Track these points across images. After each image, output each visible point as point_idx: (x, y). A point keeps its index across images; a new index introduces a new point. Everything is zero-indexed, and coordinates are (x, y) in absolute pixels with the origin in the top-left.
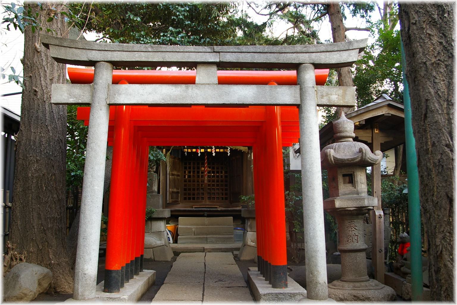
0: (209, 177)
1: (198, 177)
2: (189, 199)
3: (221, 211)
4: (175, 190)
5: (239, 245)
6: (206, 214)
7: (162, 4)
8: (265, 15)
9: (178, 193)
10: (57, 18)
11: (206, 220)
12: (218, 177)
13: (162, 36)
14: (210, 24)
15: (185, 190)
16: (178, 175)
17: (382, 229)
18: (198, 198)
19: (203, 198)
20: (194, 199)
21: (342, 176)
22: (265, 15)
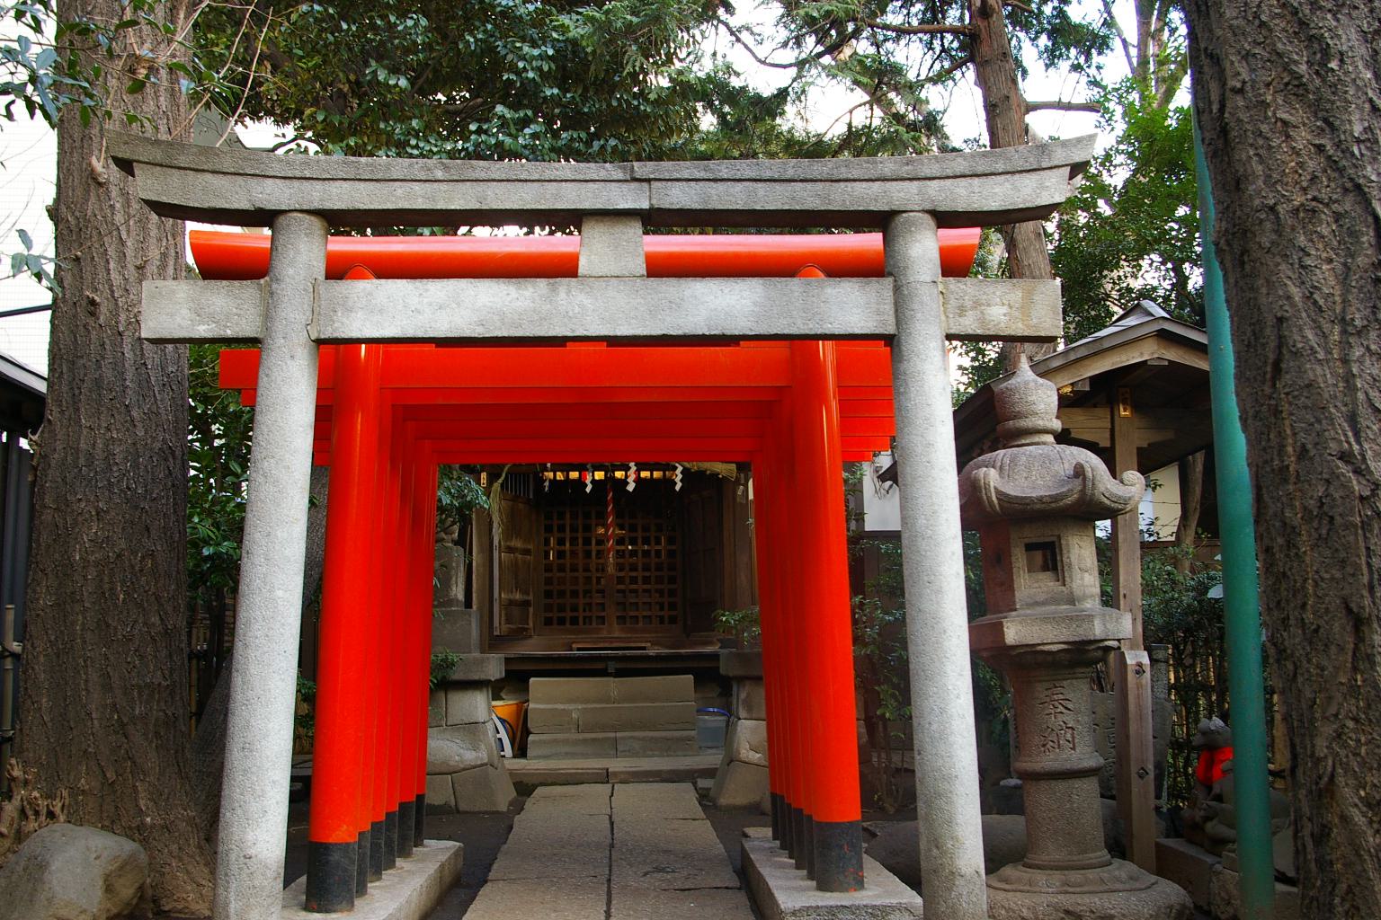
0: (620, 554)
2: (561, 621)
6: (612, 667)
12: (646, 554)
15: (548, 594)
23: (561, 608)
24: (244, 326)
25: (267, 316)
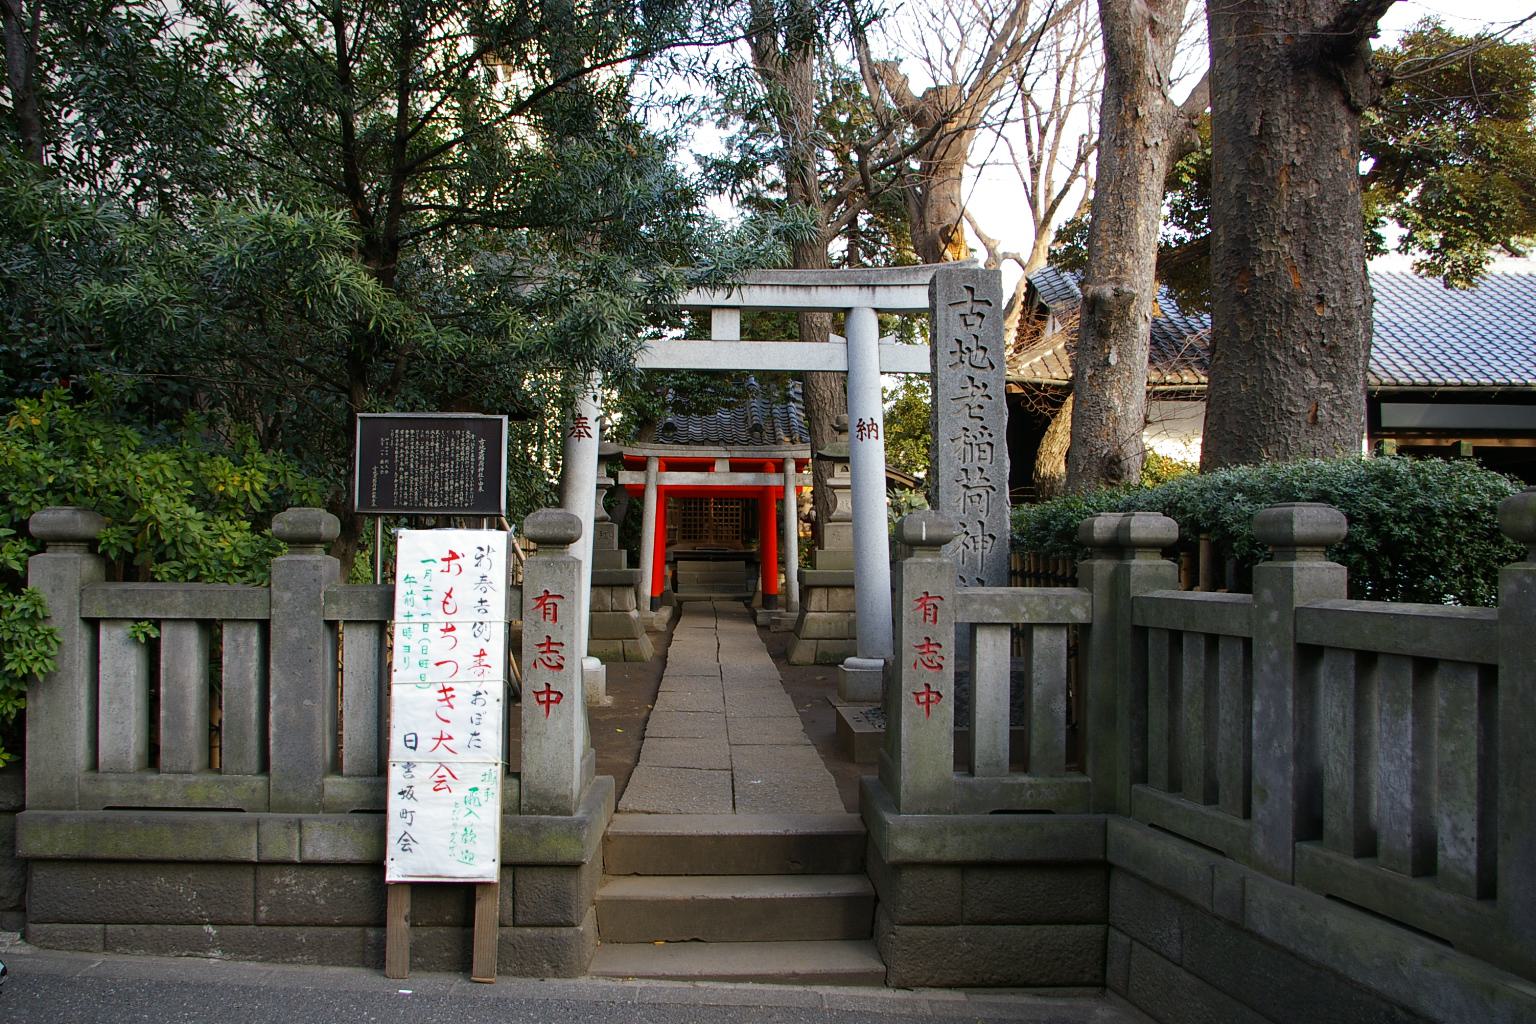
0: (715, 509)
1: (701, 509)
2: (690, 537)
3: (731, 554)
5: (750, 594)
6: (711, 557)
10: (824, 34)
11: (712, 565)
12: (726, 509)
13: (199, 69)
15: (684, 526)
18: (701, 537)
20: (695, 537)
21: (1383, 841)
23: (690, 532)
24: (642, 481)
25: (647, 480)
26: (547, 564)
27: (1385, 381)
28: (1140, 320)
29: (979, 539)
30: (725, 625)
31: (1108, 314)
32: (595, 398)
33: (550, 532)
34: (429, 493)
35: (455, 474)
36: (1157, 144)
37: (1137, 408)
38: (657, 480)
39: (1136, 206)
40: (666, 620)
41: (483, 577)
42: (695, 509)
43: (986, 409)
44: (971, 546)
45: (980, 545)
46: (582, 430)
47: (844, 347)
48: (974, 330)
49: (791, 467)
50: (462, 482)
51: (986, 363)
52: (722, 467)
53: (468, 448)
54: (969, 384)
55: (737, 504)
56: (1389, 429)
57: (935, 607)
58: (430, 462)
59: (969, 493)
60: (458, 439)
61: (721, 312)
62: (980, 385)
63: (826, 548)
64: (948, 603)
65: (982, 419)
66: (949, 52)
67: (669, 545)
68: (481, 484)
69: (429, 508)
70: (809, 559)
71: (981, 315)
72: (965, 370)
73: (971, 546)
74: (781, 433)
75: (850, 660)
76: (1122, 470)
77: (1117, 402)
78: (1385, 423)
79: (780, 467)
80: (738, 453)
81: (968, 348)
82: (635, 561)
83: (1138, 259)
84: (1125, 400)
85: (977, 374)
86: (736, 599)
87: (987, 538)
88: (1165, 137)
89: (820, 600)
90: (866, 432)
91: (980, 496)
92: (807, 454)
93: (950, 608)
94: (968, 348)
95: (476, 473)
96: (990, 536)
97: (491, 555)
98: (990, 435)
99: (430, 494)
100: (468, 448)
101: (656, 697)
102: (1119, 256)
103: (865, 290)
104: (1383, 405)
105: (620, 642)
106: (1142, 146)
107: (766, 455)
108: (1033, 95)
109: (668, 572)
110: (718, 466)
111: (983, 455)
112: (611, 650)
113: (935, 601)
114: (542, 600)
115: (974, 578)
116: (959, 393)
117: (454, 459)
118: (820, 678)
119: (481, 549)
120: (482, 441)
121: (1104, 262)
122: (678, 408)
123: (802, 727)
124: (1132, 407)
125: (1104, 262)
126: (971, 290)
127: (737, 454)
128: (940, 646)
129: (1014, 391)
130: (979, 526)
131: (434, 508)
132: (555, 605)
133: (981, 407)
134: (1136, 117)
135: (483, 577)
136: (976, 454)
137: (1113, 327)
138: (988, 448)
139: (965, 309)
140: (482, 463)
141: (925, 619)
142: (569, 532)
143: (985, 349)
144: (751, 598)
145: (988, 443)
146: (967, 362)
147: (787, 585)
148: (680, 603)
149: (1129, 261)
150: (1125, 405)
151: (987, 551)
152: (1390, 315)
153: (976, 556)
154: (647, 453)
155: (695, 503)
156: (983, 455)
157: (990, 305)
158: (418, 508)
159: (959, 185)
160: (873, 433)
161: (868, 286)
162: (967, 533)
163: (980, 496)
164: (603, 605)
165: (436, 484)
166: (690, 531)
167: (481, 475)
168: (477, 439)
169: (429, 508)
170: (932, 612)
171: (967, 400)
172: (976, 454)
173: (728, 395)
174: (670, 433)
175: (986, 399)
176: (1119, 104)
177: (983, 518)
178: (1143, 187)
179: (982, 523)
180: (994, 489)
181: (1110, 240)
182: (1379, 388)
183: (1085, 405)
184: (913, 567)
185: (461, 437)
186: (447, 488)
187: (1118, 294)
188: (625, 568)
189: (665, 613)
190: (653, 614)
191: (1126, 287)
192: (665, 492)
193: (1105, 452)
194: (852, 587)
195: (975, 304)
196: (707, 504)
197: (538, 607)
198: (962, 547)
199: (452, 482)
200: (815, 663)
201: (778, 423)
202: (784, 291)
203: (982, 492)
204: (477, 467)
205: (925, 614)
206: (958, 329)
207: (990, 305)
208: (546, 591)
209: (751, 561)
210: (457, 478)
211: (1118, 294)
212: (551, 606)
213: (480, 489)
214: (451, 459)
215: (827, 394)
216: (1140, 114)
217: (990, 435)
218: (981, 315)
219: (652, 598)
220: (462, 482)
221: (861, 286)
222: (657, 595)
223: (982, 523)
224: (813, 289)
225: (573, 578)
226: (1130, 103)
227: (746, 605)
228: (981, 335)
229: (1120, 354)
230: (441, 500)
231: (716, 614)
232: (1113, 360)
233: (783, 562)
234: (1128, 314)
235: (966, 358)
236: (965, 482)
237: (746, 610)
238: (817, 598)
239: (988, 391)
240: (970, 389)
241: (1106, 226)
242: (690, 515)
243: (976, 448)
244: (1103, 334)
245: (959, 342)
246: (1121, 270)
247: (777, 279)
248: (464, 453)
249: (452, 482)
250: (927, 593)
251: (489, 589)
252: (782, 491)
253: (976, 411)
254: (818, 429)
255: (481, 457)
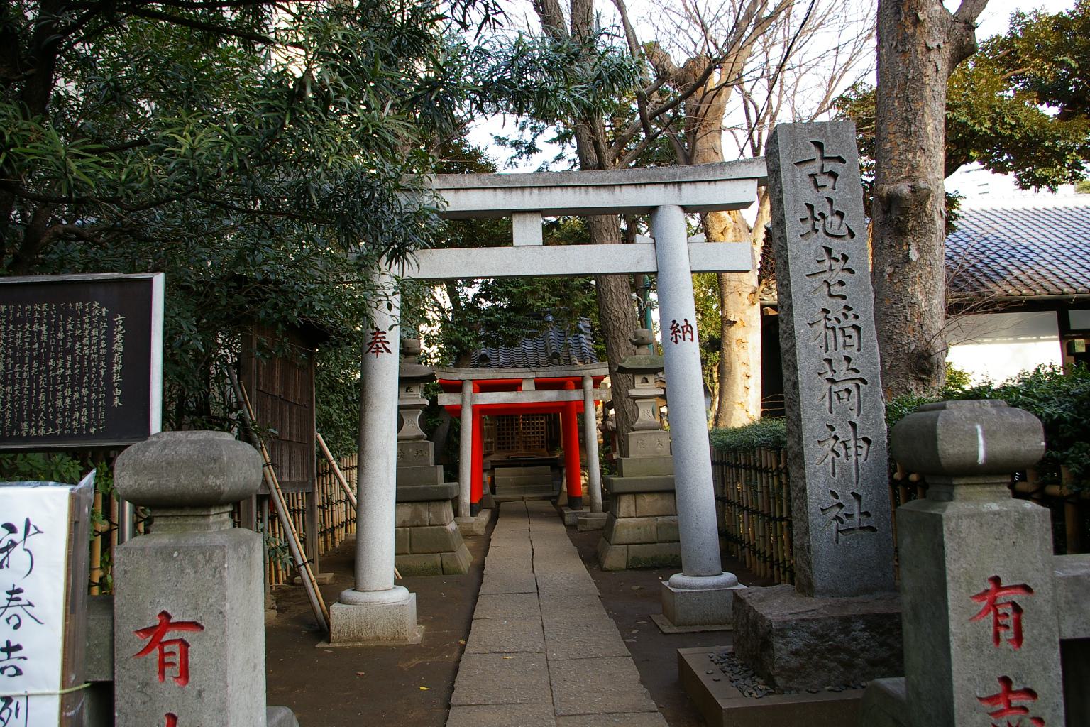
0: (524, 424)
1: (512, 424)
2: (504, 448)
3: (538, 460)
4: (489, 440)
5: (556, 493)
6: (522, 464)
7: (276, 48)
8: (736, 137)
9: (492, 442)
11: (522, 470)
12: (533, 424)
14: (358, 18)
15: (499, 439)
16: (492, 425)
17: (933, 509)
19: (518, 447)
20: (509, 448)
22: (736, 137)
25: (463, 401)
26: (165, 553)
27: (1080, 289)
28: (937, 216)
29: (851, 444)
30: (539, 526)
31: (905, 211)
32: (390, 307)
33: (172, 483)
34: (30, 412)
35: (72, 376)
36: (939, 46)
37: (939, 303)
38: (471, 400)
39: (923, 107)
40: (485, 524)
41: (14, 593)
42: (508, 425)
43: (848, 285)
44: (842, 453)
45: (852, 452)
46: (380, 345)
47: (651, 248)
48: (827, 192)
49: (589, 383)
50: (85, 391)
51: (844, 231)
52: (528, 386)
53: (95, 332)
54: (826, 257)
55: (542, 419)
56: (1076, 331)
57: (1017, 609)
58: (31, 359)
59: (835, 388)
60: (78, 317)
61: (522, 217)
62: (840, 257)
63: (631, 455)
64: (1042, 600)
65: (844, 297)
66: (696, 45)
67: (485, 456)
68: (117, 392)
69: (29, 439)
70: (611, 465)
71: (833, 175)
72: (820, 240)
73: (842, 453)
74: (575, 358)
75: (677, 578)
76: (932, 365)
77: (920, 297)
78: (1073, 327)
79: (579, 384)
80: (542, 374)
81: (821, 214)
82: (453, 473)
83: (929, 157)
84: (928, 295)
85: (835, 244)
86: (545, 498)
87: (861, 443)
88: (946, 40)
89: (628, 507)
90: (681, 334)
91: (848, 391)
92: (605, 371)
93: (1048, 609)
94: (821, 214)
95: (109, 374)
96: (865, 439)
97: (34, 541)
98: (856, 317)
99: (32, 415)
100: (95, 332)
101: (469, 630)
102: (910, 156)
103: (670, 188)
104: (1070, 311)
105: (438, 555)
106: (924, 50)
107: (567, 374)
108: (752, 97)
109: (486, 478)
110: (525, 386)
111: (849, 341)
112: (429, 564)
113: (1018, 597)
114: (155, 634)
115: (848, 493)
116: (815, 268)
117: (72, 351)
118: (635, 588)
119: (11, 528)
120: (119, 319)
121: (894, 163)
122: (489, 342)
123: (637, 676)
124: (935, 302)
125: (894, 163)
126: (819, 146)
127: (541, 375)
128: (1031, 693)
129: (770, 313)
130: (850, 428)
131: (38, 439)
132: (184, 645)
133: (841, 283)
134: (917, 22)
135: (14, 593)
136: (841, 340)
137: (910, 224)
138: (854, 333)
139: (814, 168)
140: (118, 357)
141: (997, 638)
142: (212, 481)
143: (841, 215)
144: (557, 497)
145: (854, 327)
146: (821, 230)
147: (590, 485)
148: (498, 503)
149: (921, 160)
150: (929, 300)
151: (861, 459)
152: (1068, 239)
153: (850, 466)
154: (462, 376)
155: (507, 420)
156: (849, 341)
157: (844, 162)
158: (12, 439)
159: (720, 138)
160: (688, 335)
161: (674, 183)
162: (836, 438)
163: (848, 391)
164: (422, 520)
165: (42, 397)
166: (504, 443)
167: (117, 378)
168: (110, 316)
169: (29, 439)
170: (1010, 621)
171: (825, 276)
172: (841, 340)
173: (530, 328)
174: (483, 361)
175: (848, 274)
176: (898, 12)
177: (855, 419)
178: (928, 89)
179: (853, 425)
180: (865, 382)
181: (899, 141)
182: (1076, 296)
183: (887, 303)
184: (965, 523)
185: (83, 313)
186: (59, 403)
187: (915, 190)
188: (441, 483)
189: (484, 517)
190: (473, 519)
191: (922, 184)
192: (479, 411)
193: (913, 347)
194: (673, 492)
195: (826, 163)
196: (517, 420)
197: (148, 649)
198: (832, 455)
199: (68, 392)
200: (628, 568)
201: (572, 351)
202: (587, 192)
203: (851, 385)
204: (110, 364)
205: (997, 624)
206: (808, 192)
207: (844, 162)
208: (165, 615)
209: (556, 466)
210: (76, 384)
211: (915, 190)
212: (176, 648)
213: (117, 401)
214: (67, 352)
215: (621, 315)
216: (921, 18)
217: (856, 317)
218: (833, 175)
219: (471, 504)
220: (85, 391)
221: (666, 184)
222: (477, 502)
223: (853, 425)
224: (617, 189)
225: (222, 582)
226: (910, 10)
227: (554, 504)
228: (835, 197)
229: (919, 250)
230: (50, 423)
231: (528, 514)
232: (914, 255)
233: (586, 466)
234: (925, 211)
235: (819, 226)
236: (829, 375)
237: (553, 509)
238: (625, 505)
239: (848, 265)
240: (827, 263)
241: (893, 129)
242: (503, 429)
243: (839, 334)
244: (900, 232)
245: (810, 207)
246: (913, 168)
247: (579, 180)
248: (89, 340)
249: (68, 392)
250: (996, 580)
251: (26, 620)
252: (582, 405)
253: (836, 289)
254: (614, 346)
255: (118, 346)
